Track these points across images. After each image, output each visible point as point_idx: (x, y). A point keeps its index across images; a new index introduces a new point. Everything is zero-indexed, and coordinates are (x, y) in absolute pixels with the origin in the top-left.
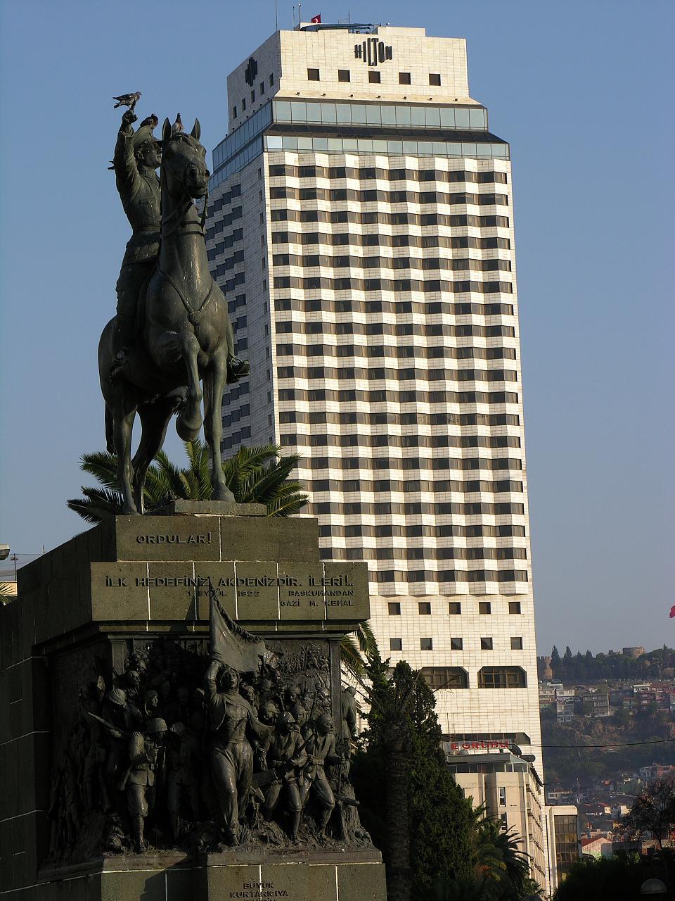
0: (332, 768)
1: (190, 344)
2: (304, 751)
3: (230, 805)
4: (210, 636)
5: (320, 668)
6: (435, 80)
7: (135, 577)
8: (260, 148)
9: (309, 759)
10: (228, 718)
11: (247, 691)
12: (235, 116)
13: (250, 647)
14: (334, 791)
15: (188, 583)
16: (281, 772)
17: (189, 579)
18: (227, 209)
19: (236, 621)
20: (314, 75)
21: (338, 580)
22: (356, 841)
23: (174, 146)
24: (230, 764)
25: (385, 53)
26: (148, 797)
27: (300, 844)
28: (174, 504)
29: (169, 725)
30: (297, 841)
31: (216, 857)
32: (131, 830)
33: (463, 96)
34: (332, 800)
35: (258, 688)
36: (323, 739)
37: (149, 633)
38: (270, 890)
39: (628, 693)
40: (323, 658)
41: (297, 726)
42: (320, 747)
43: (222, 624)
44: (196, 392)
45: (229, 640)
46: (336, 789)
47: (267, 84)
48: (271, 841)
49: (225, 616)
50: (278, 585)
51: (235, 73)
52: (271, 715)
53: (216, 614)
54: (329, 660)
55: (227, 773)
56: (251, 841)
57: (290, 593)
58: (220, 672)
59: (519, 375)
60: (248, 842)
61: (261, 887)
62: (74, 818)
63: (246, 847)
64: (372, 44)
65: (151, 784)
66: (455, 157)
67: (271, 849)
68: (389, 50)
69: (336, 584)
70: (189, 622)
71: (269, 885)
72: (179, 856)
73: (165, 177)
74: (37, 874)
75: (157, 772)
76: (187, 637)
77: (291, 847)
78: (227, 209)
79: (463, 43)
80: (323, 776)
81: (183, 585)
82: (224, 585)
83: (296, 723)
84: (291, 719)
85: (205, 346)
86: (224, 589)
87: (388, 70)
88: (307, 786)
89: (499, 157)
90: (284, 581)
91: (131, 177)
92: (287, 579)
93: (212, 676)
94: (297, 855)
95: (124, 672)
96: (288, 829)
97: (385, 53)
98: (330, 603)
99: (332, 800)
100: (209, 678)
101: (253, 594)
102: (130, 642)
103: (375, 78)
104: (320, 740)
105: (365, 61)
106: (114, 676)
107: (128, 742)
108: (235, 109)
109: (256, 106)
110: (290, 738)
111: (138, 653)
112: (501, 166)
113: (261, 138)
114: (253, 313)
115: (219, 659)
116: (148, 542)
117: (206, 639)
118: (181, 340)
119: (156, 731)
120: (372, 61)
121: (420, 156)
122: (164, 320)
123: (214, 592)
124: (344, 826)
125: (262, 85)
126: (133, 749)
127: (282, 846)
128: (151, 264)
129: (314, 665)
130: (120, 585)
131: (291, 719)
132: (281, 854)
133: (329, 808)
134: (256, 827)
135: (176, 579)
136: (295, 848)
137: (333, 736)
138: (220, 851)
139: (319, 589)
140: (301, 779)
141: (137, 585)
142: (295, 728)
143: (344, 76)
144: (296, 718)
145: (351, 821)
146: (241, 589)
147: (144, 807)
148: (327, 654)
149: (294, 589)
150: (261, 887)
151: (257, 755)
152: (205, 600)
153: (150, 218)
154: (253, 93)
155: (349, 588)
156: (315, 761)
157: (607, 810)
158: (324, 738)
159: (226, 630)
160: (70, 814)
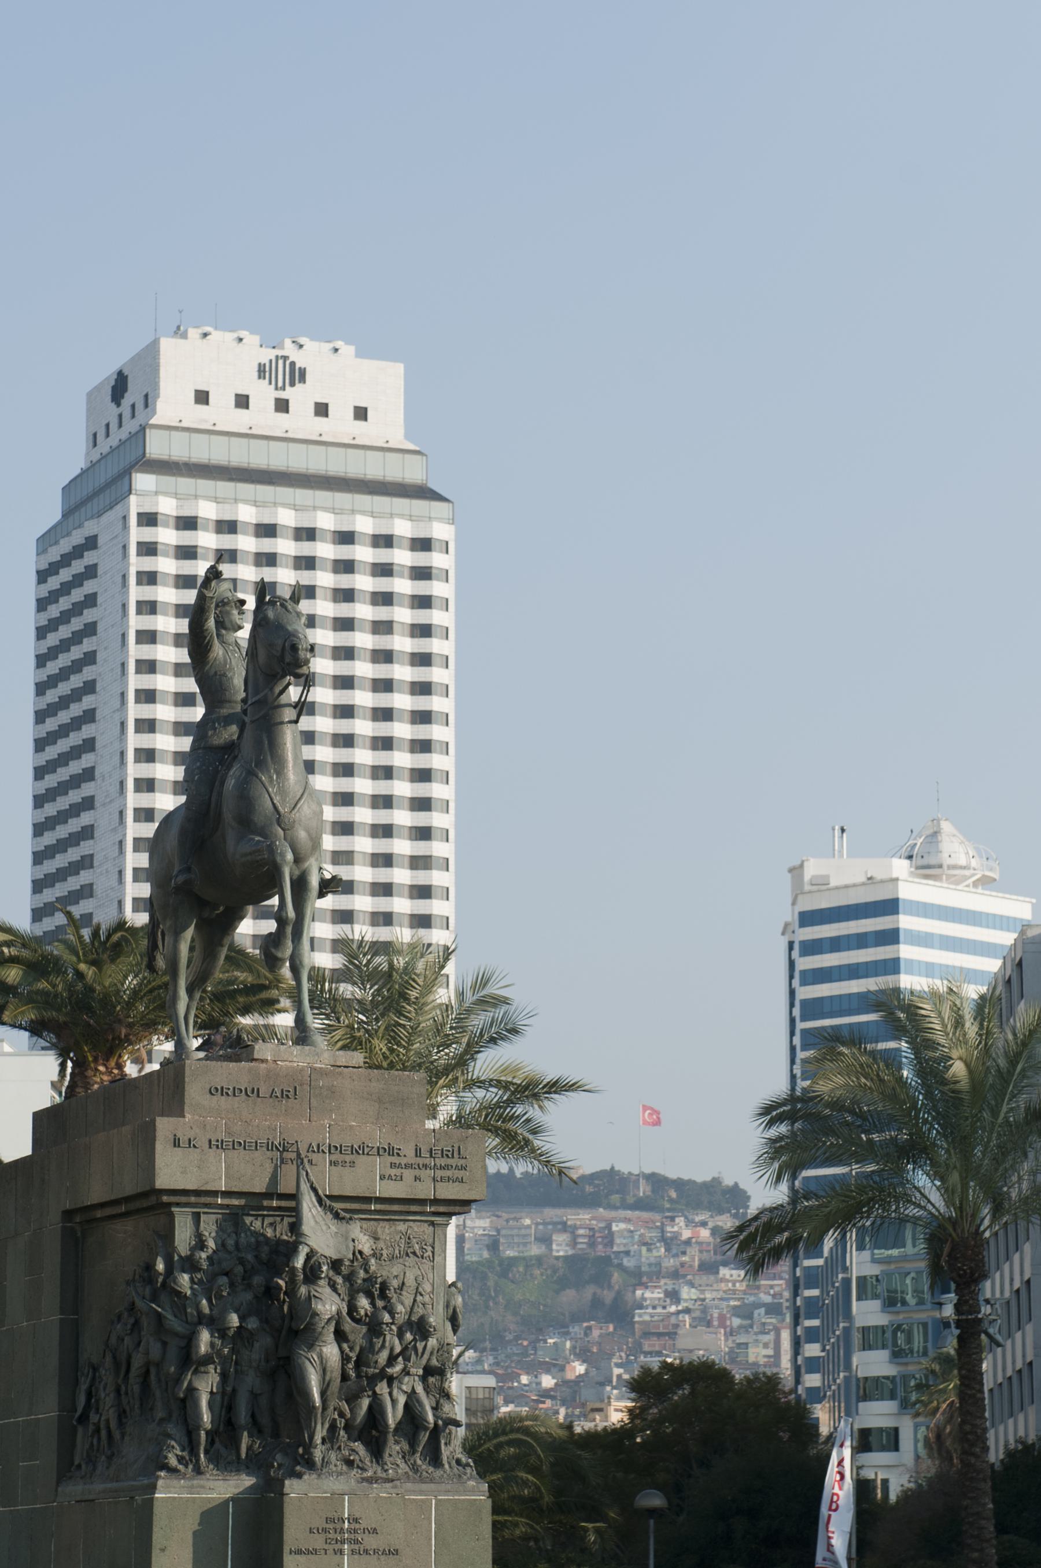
0: (431, 1380)
1: (283, 855)
2: (400, 1358)
3: (313, 1420)
4: (296, 1212)
5: (422, 1257)
6: (361, 413)
7: (208, 1137)
8: (127, 488)
9: (406, 1367)
10: (315, 1314)
11: (335, 1282)
12: (95, 445)
13: (343, 1226)
14: (433, 1408)
15: (270, 1147)
16: (373, 1380)
17: (272, 1143)
18: (78, 566)
19: (326, 1196)
20: (202, 397)
21: (449, 1151)
22: (456, 1469)
23: (271, 614)
24: (313, 1370)
25: (297, 375)
26: (211, 1405)
27: (390, 1471)
28: (254, 1048)
29: (241, 1318)
30: (386, 1467)
31: (294, 1483)
32: (192, 1446)
33: (398, 439)
34: (431, 1418)
35: (349, 1278)
36: (424, 1343)
37: (221, 1206)
38: (357, 1526)
39: (559, 1227)
40: (426, 1245)
41: (394, 1327)
42: (420, 1354)
43: (311, 1198)
44: (287, 913)
45: (319, 1219)
46: (434, 1405)
47: (140, 406)
48: (358, 1467)
49: (314, 1190)
50: (378, 1154)
51: (97, 389)
52: (362, 1312)
53: (305, 1187)
54: (433, 1248)
55: (310, 1382)
56: (336, 1466)
57: (393, 1165)
58: (309, 1257)
59: (452, 805)
60: (332, 1467)
61: (346, 1521)
62: (113, 1424)
63: (330, 1474)
64: (281, 362)
65: (215, 1390)
66: (382, 515)
67: (358, 1475)
68: (303, 373)
69: (447, 1155)
70: (268, 1195)
71: (356, 1520)
72: (247, 1481)
73: (256, 649)
74: (56, 1491)
75: (224, 1376)
76: (265, 1213)
77: (380, 1473)
78: (78, 566)
79: (400, 368)
80: (420, 1389)
81: (265, 1149)
82: (314, 1152)
83: (392, 1324)
84: (387, 1318)
85: (298, 860)
86: (314, 1157)
87: (300, 397)
88: (402, 1400)
89: (440, 520)
90: (385, 1149)
91: (208, 643)
92: (389, 1148)
93: (299, 1262)
94: (390, 1484)
95: (189, 1253)
96: (377, 1451)
97: (297, 375)
98: (439, 1179)
99: (431, 1418)
100: (296, 1265)
101: (348, 1164)
102: (197, 1217)
103: (282, 406)
104: (420, 1346)
105: (270, 383)
106: (176, 1258)
107: (190, 1340)
108: (95, 435)
109: (123, 434)
110: (384, 1341)
111: (205, 1229)
112: (441, 531)
113: (127, 477)
114: (105, 703)
115: (308, 1242)
116: (222, 1095)
117: (288, 1216)
118: (271, 849)
119: (227, 1326)
120: (280, 384)
121: (336, 511)
122: (246, 822)
123: (302, 1160)
124: (443, 1451)
125: (133, 406)
126: (198, 1347)
127: (370, 1474)
128: (230, 749)
129: (414, 1253)
130: (190, 1147)
131: (387, 1318)
132: (372, 1483)
133: (426, 1429)
134: (339, 1448)
135: (256, 1142)
136: (384, 1475)
137: (435, 1341)
138: (299, 1476)
139: (427, 1161)
140: (395, 1391)
141: (210, 1147)
142: (391, 1330)
143: (242, 402)
144: (393, 1318)
145: (452, 1445)
146: (334, 1158)
147: (206, 1417)
148: (431, 1240)
149: (395, 1160)
150: (346, 1521)
151: (345, 1359)
152: (290, 1170)
153: (227, 693)
154: (120, 416)
155: (462, 1162)
156: (413, 1371)
157: (525, 1379)
158: (424, 1343)
159: (315, 1206)
160: (108, 1421)
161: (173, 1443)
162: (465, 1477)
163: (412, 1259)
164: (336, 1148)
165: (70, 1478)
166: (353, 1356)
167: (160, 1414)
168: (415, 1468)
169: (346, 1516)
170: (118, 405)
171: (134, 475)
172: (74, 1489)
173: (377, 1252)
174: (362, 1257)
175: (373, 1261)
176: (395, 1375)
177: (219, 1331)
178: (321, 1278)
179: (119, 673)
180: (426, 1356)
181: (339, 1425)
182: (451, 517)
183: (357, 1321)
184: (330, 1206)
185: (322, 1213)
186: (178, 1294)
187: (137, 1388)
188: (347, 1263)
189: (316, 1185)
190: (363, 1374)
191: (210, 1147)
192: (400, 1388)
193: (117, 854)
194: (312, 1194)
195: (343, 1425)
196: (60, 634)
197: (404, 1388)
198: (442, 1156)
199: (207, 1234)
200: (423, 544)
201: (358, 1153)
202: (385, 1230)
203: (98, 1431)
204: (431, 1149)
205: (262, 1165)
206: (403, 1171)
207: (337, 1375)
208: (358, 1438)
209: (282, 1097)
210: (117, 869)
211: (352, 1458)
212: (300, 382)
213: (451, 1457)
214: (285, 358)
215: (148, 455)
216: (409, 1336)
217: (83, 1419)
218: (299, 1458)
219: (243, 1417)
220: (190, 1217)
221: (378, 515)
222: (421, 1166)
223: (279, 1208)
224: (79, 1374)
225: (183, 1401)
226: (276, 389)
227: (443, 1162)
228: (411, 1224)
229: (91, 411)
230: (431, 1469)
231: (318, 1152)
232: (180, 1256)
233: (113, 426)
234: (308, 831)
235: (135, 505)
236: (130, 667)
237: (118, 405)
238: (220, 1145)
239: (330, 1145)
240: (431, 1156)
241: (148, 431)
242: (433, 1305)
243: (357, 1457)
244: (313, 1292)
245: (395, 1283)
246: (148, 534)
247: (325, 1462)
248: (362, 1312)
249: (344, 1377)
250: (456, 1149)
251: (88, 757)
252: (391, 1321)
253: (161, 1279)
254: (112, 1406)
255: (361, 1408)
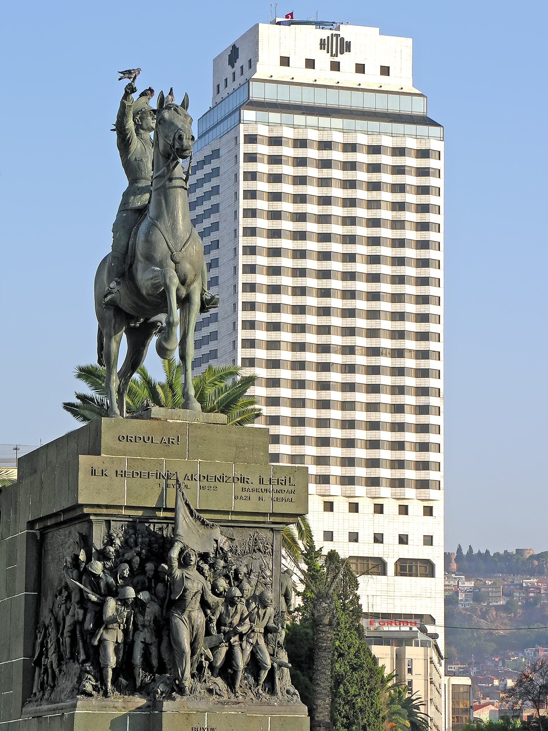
5: (265, 552)
6: (385, 71)
8: (238, 119)
9: (251, 627)
11: (203, 569)
13: (208, 531)
14: (271, 655)
15: (158, 476)
17: (160, 473)
20: (285, 61)
21: (283, 480)
25: (345, 47)
27: (241, 697)
28: (151, 410)
29: (137, 592)
30: (237, 694)
32: (101, 678)
36: (264, 611)
37: (125, 516)
39: (518, 587)
40: (267, 544)
42: (261, 618)
45: (191, 525)
46: (272, 653)
47: (246, 68)
48: (217, 693)
49: (188, 505)
51: (220, 56)
53: (181, 503)
54: (272, 546)
60: (197, 693)
62: (55, 665)
64: (334, 38)
66: (398, 135)
67: (216, 699)
68: (349, 44)
69: (281, 484)
74: (22, 711)
77: (233, 699)
80: (262, 642)
82: (189, 480)
83: (242, 597)
84: (238, 593)
86: (189, 483)
88: (249, 649)
91: (129, 138)
93: (175, 554)
94: (237, 706)
96: (231, 683)
97: (345, 47)
99: (269, 661)
100: (172, 556)
101: (212, 488)
103: (336, 67)
104: (261, 612)
105: (328, 52)
106: (94, 551)
107: (101, 606)
108: (218, 86)
109: (236, 85)
112: (436, 145)
116: (127, 441)
117: (171, 523)
120: (334, 52)
123: (180, 485)
124: (277, 684)
125: (242, 67)
127: (225, 698)
128: (142, 211)
129: (259, 550)
133: (265, 669)
134: (205, 681)
135: (149, 473)
136: (236, 700)
137: (272, 609)
140: (244, 644)
141: (117, 476)
143: (310, 64)
146: (203, 484)
149: (246, 486)
152: (172, 492)
154: (234, 73)
156: (256, 629)
157: (496, 683)
158: (265, 610)
160: (52, 662)
161: (89, 676)
162: (292, 702)
163: (258, 554)
164: (204, 477)
165: (30, 702)
166: (215, 618)
167: (82, 657)
168: (258, 695)
169: (206, 727)
170: (233, 67)
171: (242, 111)
172: (31, 708)
173: (234, 549)
174: (222, 552)
175: (230, 554)
176: (243, 632)
177: (120, 600)
178: (191, 565)
179: (233, 236)
180: (266, 619)
181: (204, 666)
182: (442, 136)
183: (218, 595)
184: (198, 516)
185: (194, 522)
186: (94, 575)
187: (68, 640)
188: (212, 556)
189: (189, 502)
190: (222, 631)
191: (117, 476)
192: (247, 641)
193: (232, 349)
194: (186, 508)
195: (207, 665)
196: (197, 212)
197: (251, 640)
198: (278, 484)
199: (115, 535)
200: (424, 154)
201: (220, 481)
202: (237, 534)
203: (46, 670)
204: (270, 479)
205: (152, 488)
206: (250, 493)
207: (202, 631)
208: (219, 675)
209: (169, 443)
210: (232, 359)
211: (211, 688)
212: (346, 51)
213: (283, 688)
214: (337, 36)
215: (251, 98)
216: (253, 605)
217: (38, 663)
218: (175, 687)
219: (138, 659)
220: (104, 523)
221: (396, 135)
222: (263, 490)
223: (166, 518)
224: (37, 631)
225: (98, 646)
226: (332, 56)
227: (280, 487)
228: (258, 530)
229: (216, 71)
230: (268, 696)
231: (192, 480)
232: (96, 550)
233: (230, 80)
234: (191, 263)
235: (243, 130)
236: (240, 232)
237: (233, 67)
238: (124, 474)
239: (200, 475)
240: (270, 484)
241: (251, 83)
242: (272, 584)
243: (217, 688)
244: (185, 574)
245: (244, 570)
246: (251, 148)
247: (192, 691)
248: (222, 589)
249: (208, 633)
250: (288, 480)
251: (214, 289)
252: (241, 595)
253: (83, 565)
254: (54, 653)
255: (221, 654)
